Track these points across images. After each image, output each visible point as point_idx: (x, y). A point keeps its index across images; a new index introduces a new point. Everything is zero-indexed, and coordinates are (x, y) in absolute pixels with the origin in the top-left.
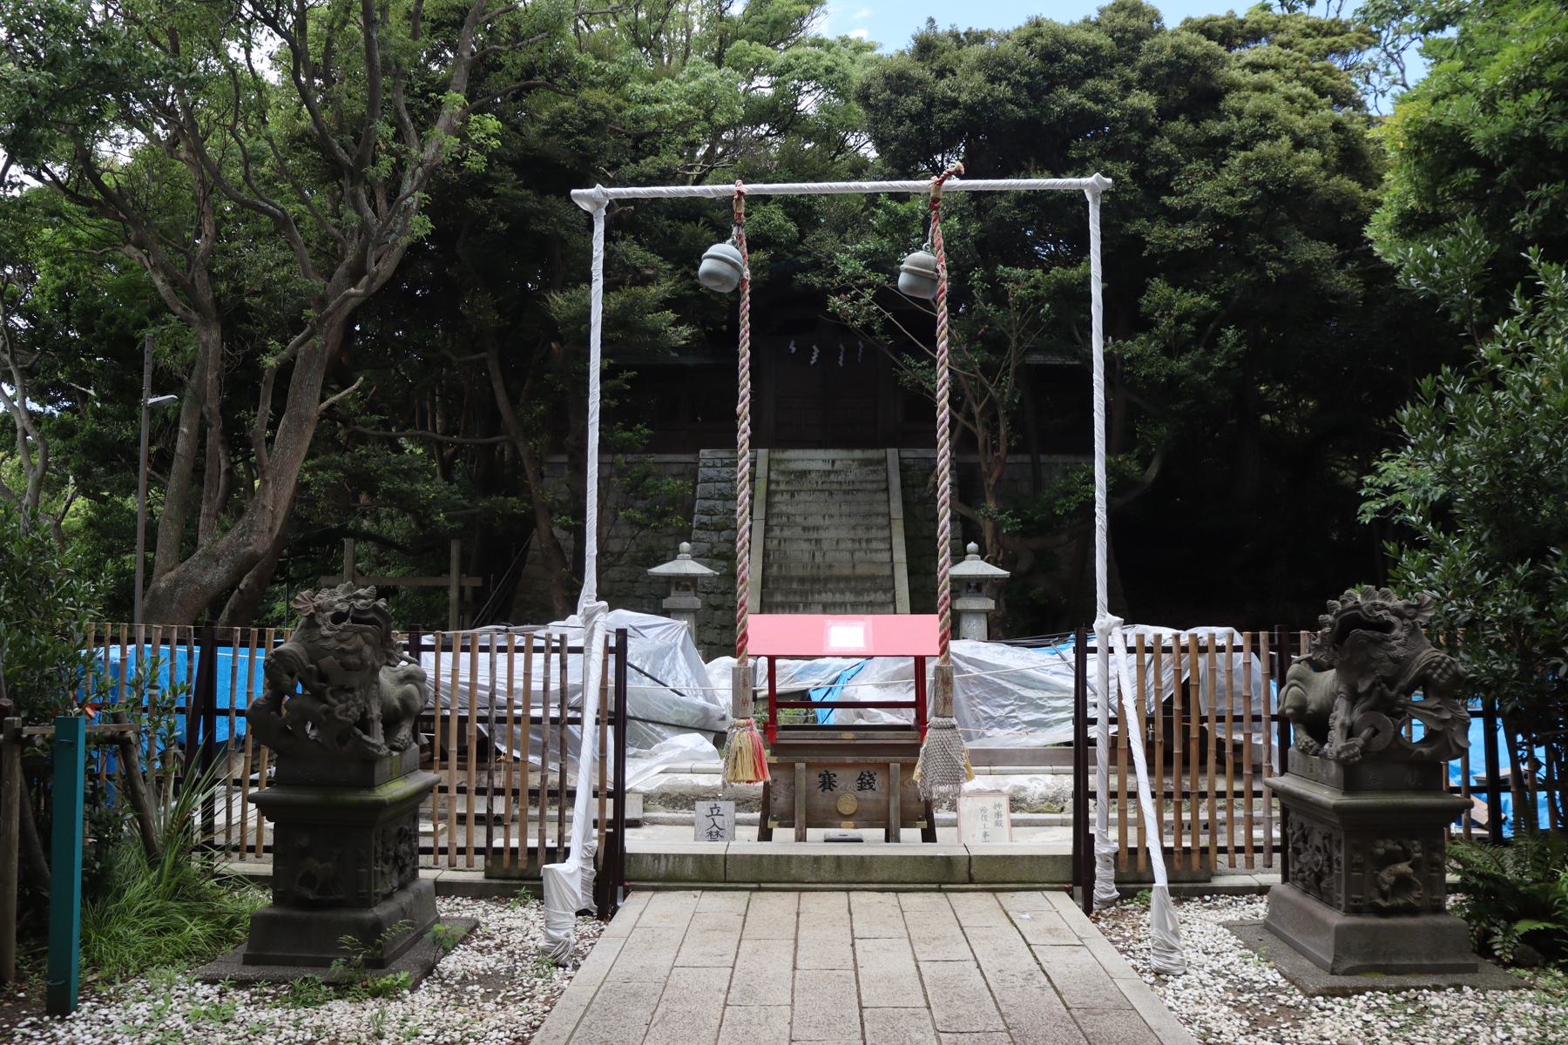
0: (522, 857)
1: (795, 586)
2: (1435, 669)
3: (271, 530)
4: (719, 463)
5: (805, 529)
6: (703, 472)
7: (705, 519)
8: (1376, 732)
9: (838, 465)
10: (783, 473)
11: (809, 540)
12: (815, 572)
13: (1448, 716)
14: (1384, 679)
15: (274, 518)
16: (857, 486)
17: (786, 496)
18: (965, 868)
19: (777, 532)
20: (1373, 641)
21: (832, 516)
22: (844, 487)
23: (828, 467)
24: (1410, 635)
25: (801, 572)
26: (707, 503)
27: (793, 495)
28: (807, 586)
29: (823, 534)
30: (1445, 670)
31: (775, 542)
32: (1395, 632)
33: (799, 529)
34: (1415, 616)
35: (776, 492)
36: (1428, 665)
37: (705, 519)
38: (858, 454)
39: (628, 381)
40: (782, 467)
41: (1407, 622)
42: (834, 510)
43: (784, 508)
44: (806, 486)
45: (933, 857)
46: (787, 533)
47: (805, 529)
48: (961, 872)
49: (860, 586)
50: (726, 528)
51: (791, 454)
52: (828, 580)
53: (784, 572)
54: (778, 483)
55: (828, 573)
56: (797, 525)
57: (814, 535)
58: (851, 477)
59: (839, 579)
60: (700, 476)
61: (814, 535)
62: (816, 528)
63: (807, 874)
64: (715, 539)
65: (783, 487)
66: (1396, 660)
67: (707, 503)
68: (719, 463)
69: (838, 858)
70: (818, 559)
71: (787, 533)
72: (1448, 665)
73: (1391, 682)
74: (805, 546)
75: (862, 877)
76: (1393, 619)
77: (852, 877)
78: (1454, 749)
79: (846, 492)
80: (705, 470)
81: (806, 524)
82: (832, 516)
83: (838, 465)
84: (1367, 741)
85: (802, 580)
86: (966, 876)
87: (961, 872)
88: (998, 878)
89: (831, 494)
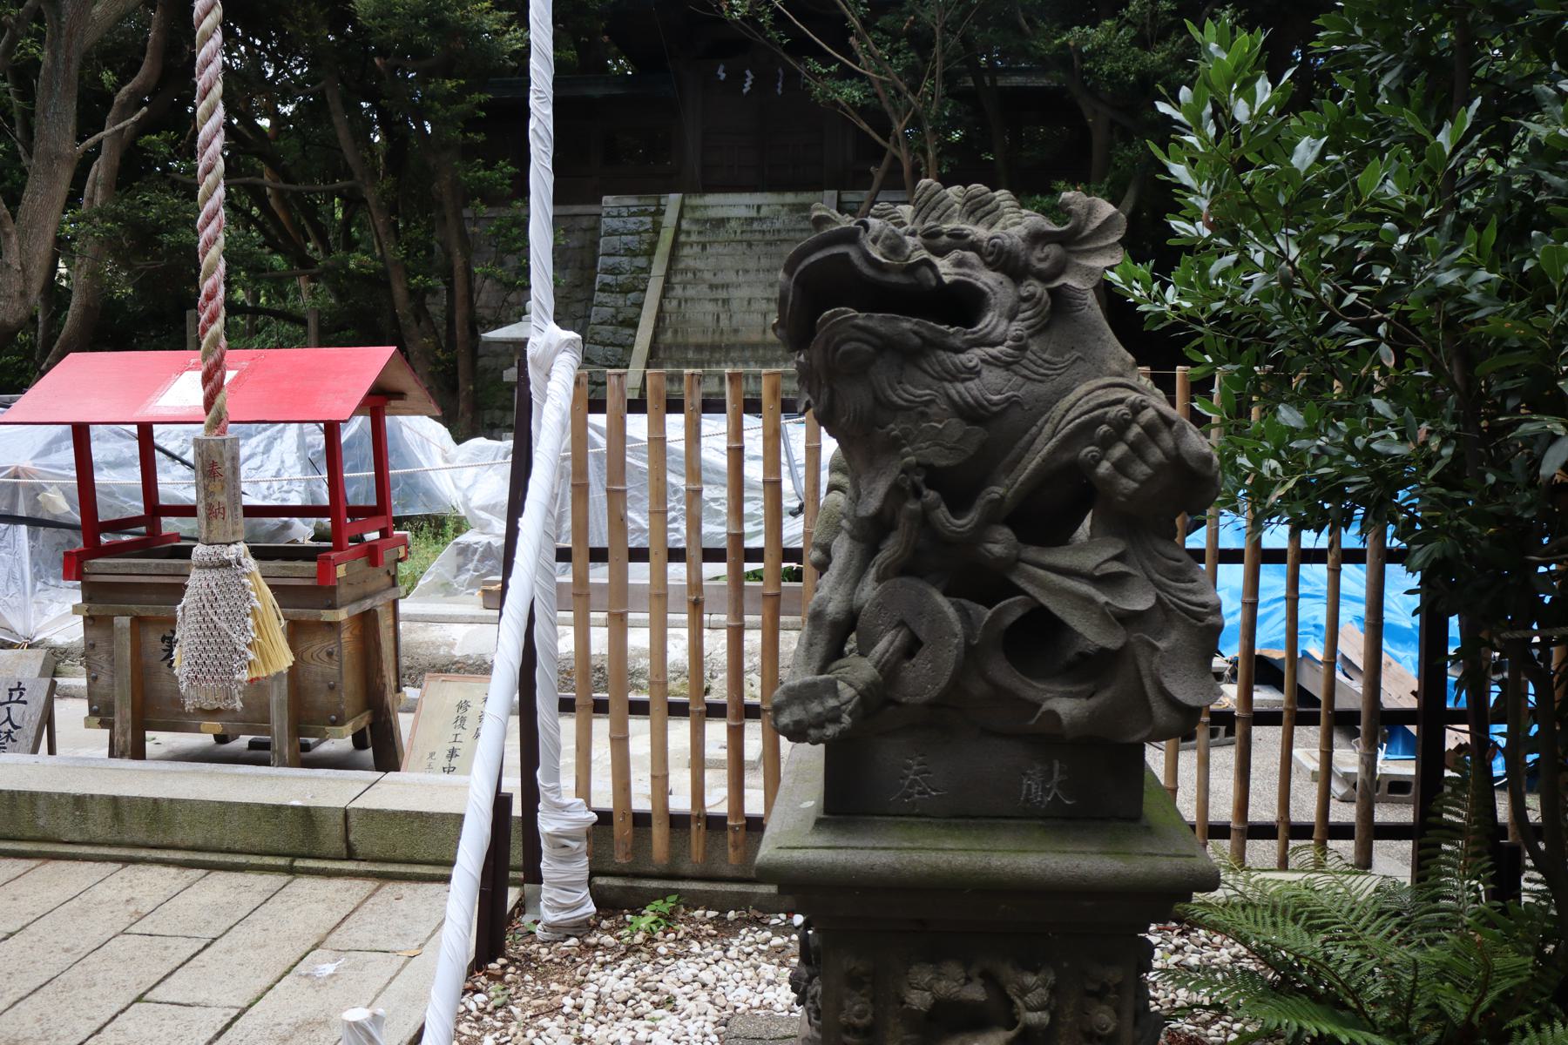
0: (659, 832)
1: (690, 355)
2: (1106, 444)
3: (23, 294)
4: (624, 212)
5: (712, 287)
6: (607, 223)
7: (609, 279)
8: (912, 647)
9: (764, 212)
10: (697, 221)
11: (716, 300)
12: (717, 338)
13: (1141, 602)
14: (934, 476)
15: (27, 280)
16: (783, 236)
17: (697, 249)
18: (338, 831)
19: (678, 291)
20: (889, 346)
21: (746, 271)
22: (768, 237)
23: (753, 214)
24: (1038, 331)
25: (700, 339)
26: (611, 261)
27: (704, 247)
28: (706, 355)
29: (735, 293)
30: (1137, 449)
31: (675, 303)
32: (991, 321)
33: (704, 288)
34: (1060, 268)
35: (684, 244)
36: (1084, 431)
37: (609, 279)
38: (790, 198)
39: (480, 106)
40: (698, 215)
41: (1034, 287)
42: (752, 265)
43: (691, 263)
44: (722, 235)
45: (278, 809)
46: (691, 292)
47: (712, 287)
48: (332, 837)
49: (769, 355)
50: (634, 289)
51: (710, 199)
52: (729, 348)
53: (680, 339)
54: (688, 233)
55: (733, 339)
56: (704, 281)
57: (722, 294)
58: (778, 225)
59: (744, 346)
60: (603, 227)
61: (722, 294)
62: (726, 286)
63: (66, 828)
64: (621, 302)
65: (694, 238)
66: (973, 413)
67: (611, 261)
68: (624, 212)
69: (115, 800)
70: (724, 322)
71: (691, 292)
72: (1151, 431)
73: (958, 487)
74: (710, 307)
75: (158, 838)
76: (986, 279)
77: (141, 836)
78: (1160, 711)
79: (769, 243)
80: (608, 220)
81: (716, 281)
82: (746, 271)
83: (764, 212)
84: (890, 671)
85: (699, 348)
86: (339, 846)
87: (332, 837)
88: (399, 854)
89: (750, 245)
